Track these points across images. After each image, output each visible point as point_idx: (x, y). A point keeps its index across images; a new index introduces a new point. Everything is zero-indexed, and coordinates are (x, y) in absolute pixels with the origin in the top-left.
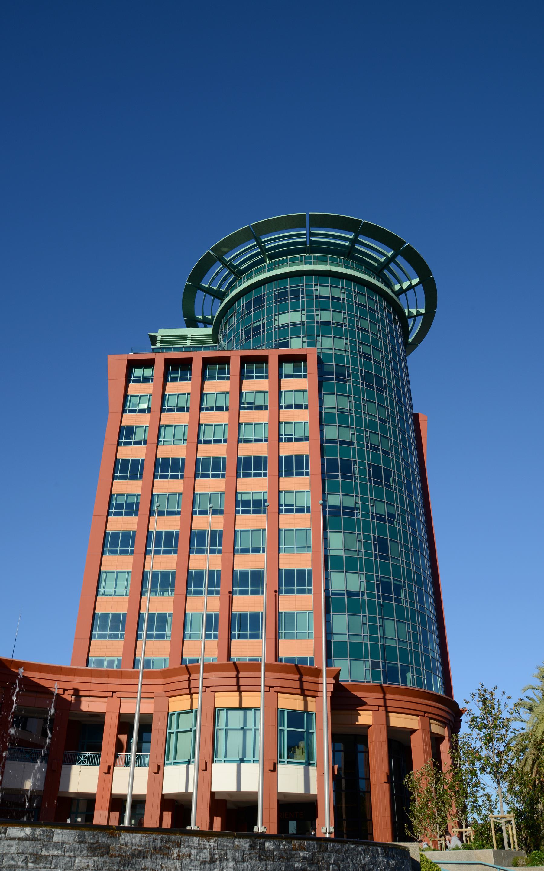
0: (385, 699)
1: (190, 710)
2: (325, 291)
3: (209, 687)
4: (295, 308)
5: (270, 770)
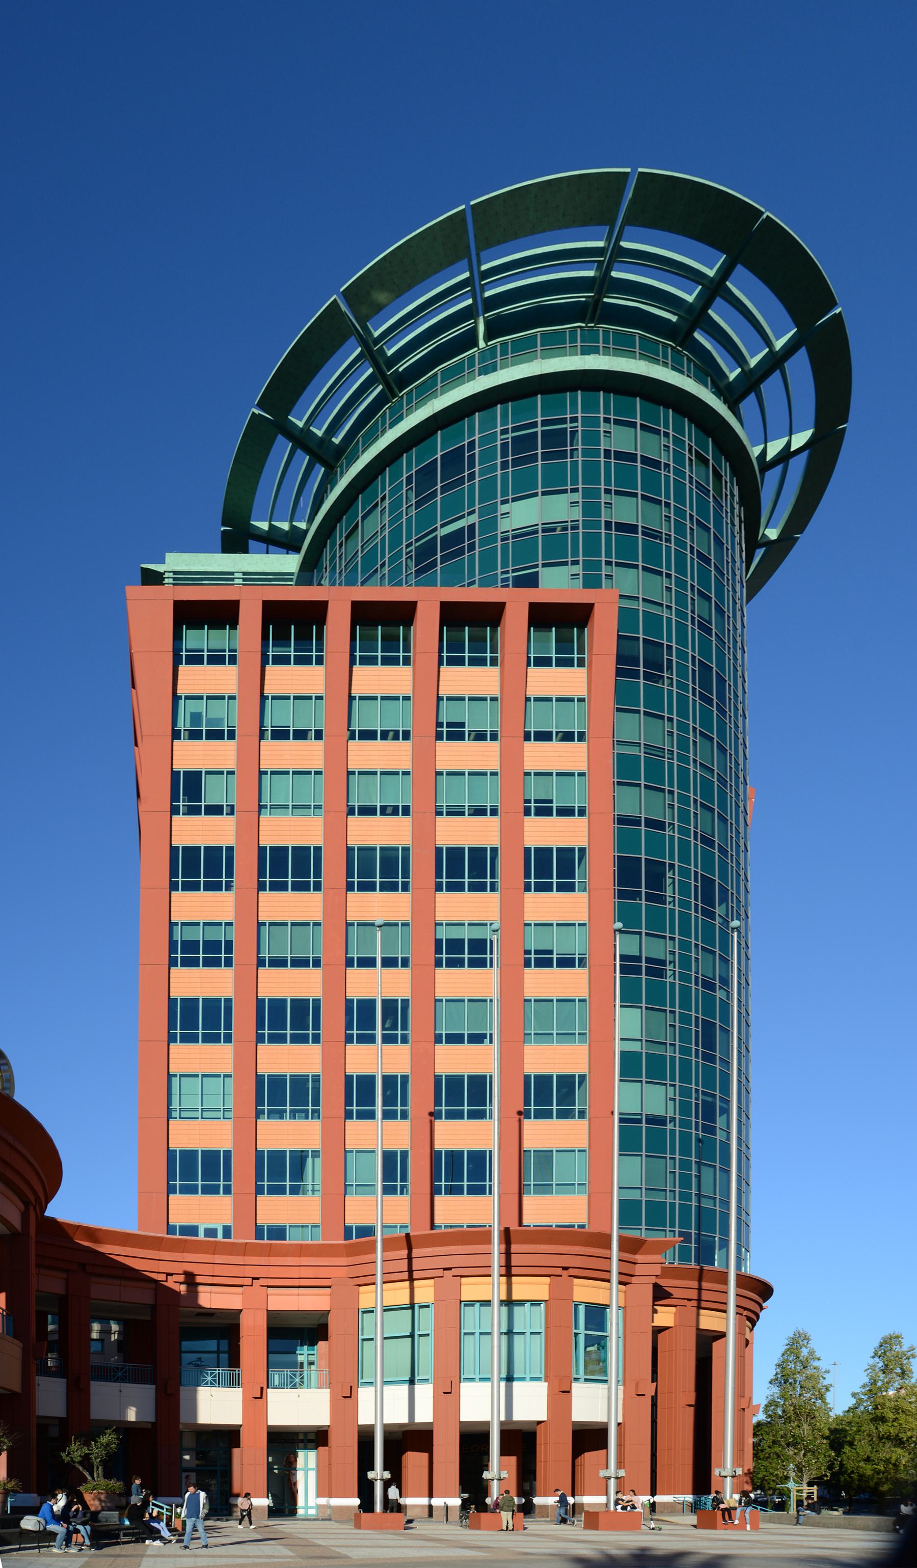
1: (409, 1306)
3: (258, 1279)
5: (256, 1398)
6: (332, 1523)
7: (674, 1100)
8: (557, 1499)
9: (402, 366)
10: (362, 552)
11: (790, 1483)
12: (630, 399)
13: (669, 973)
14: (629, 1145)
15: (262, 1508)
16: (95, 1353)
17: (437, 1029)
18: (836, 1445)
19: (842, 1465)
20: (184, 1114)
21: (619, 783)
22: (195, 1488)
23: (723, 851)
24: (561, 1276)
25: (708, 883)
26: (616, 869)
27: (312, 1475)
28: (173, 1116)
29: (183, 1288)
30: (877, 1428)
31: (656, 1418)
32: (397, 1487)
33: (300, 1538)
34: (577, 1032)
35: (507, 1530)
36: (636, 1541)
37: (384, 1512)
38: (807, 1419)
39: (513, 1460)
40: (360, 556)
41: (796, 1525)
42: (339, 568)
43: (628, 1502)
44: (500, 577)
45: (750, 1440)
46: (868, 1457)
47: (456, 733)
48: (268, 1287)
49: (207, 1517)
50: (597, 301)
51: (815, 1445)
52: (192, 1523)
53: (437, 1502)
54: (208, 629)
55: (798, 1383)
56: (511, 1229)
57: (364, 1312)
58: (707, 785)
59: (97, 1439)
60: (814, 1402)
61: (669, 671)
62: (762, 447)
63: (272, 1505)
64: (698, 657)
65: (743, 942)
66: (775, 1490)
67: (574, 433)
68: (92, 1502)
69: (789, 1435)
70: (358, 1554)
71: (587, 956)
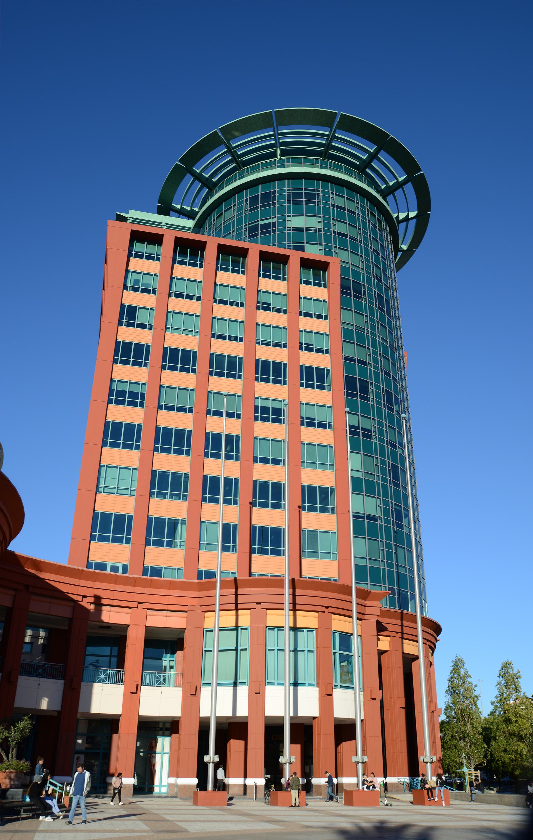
0: (402, 626)
1: (235, 628)
2: (339, 201)
3: (141, 603)
4: (311, 214)
6: (178, 800)
7: (380, 507)
8: (327, 779)
9: (245, 159)
10: (224, 224)
11: (464, 768)
12: (342, 188)
13: (374, 437)
14: (358, 532)
15: (129, 786)
16: (26, 653)
17: (255, 454)
18: (487, 740)
19: (492, 755)
20: (106, 490)
21: (344, 341)
22: (82, 768)
23: (395, 379)
24: (324, 612)
25: (389, 394)
26: (345, 381)
27: (166, 757)
28: (100, 491)
29: (92, 607)
30: (507, 728)
31: (384, 717)
32: (223, 769)
33: (155, 814)
34: (329, 464)
35: (295, 806)
36: (377, 815)
37: (214, 790)
38: (469, 720)
39: (298, 747)
40: (223, 226)
41: (471, 802)
42: (213, 229)
43: (371, 782)
44: (287, 245)
45: (439, 735)
46: (505, 749)
47: (266, 307)
48: (148, 609)
49: (88, 796)
50: (326, 152)
51: (475, 740)
52: (77, 800)
53: (250, 782)
54: (147, 244)
55: (461, 693)
56: (295, 579)
57: (207, 631)
58: (385, 349)
59: (17, 724)
60: (471, 708)
61: (365, 295)
62: (397, 214)
63: (136, 784)
64: (388, 424)
65: (408, 425)
66: (456, 773)
67: (318, 196)
68: (4, 781)
69: (460, 732)
70: (194, 828)
71: (332, 423)
